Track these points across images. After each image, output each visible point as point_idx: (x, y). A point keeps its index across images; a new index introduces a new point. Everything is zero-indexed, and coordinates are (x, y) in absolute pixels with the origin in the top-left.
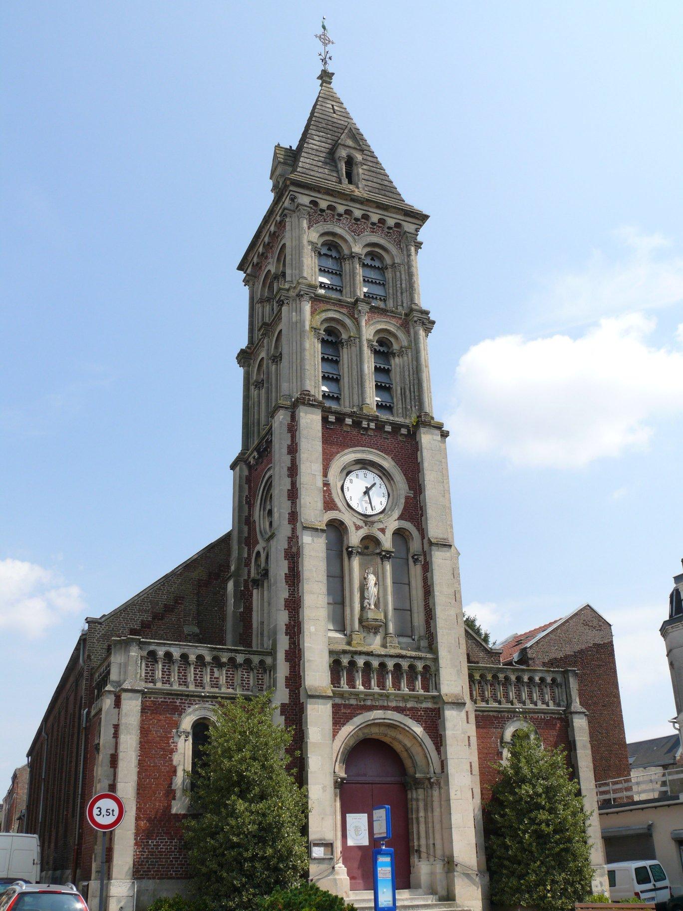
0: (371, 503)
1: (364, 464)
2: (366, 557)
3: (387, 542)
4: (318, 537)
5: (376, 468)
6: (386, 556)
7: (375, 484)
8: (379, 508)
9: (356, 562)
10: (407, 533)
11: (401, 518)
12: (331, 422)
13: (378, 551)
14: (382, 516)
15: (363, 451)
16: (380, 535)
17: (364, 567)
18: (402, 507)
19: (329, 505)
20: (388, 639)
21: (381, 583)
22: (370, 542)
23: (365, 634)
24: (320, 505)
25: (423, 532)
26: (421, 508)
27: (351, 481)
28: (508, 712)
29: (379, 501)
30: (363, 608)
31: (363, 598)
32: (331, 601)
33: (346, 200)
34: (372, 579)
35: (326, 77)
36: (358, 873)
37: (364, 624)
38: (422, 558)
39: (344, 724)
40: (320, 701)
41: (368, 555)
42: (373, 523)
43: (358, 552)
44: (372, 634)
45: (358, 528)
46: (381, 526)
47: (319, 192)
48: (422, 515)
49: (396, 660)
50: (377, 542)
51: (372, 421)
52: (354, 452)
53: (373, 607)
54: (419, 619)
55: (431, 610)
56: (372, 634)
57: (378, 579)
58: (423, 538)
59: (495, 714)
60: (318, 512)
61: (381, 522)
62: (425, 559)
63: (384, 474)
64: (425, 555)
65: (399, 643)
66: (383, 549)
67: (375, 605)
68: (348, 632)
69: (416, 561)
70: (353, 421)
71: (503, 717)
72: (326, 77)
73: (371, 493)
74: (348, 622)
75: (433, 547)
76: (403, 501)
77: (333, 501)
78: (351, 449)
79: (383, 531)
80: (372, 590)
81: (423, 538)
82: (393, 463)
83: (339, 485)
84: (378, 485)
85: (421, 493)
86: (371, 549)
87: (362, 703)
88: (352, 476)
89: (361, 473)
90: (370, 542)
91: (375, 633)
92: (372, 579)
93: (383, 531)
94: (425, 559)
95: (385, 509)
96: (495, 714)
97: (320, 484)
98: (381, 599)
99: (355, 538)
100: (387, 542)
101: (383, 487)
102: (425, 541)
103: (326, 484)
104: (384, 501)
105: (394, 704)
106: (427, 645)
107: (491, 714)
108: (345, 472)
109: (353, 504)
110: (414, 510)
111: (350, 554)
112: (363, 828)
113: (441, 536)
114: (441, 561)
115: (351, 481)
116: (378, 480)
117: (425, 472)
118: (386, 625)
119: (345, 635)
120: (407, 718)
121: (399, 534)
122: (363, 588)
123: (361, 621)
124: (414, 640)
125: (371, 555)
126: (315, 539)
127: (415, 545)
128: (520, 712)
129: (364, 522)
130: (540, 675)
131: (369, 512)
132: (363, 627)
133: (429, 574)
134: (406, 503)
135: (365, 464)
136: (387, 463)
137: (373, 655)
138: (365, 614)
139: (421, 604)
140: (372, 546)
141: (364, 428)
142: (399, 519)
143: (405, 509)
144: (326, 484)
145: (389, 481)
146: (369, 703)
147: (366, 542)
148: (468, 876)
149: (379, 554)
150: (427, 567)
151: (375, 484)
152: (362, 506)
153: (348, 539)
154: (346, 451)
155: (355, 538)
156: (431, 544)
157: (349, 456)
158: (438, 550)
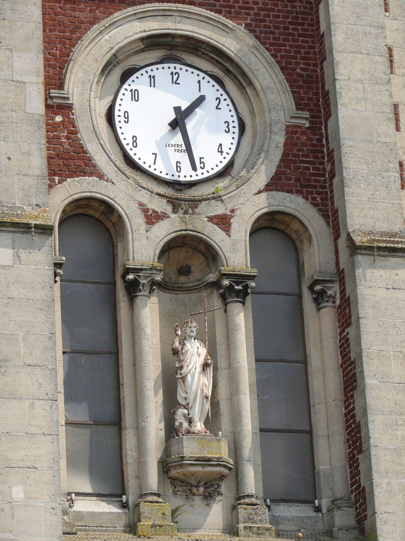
0: (189, 150)
1: (171, 48)
2: (183, 296)
3: (235, 252)
4: (31, 246)
5: (202, 55)
6: (235, 289)
7: (200, 100)
8: (214, 163)
9: (150, 312)
10: (295, 226)
11: (274, 185)
13: (212, 277)
14: (222, 184)
15: (165, 14)
16: (215, 236)
17: (172, 323)
18: (276, 156)
19: (67, 158)
20: (242, 512)
21: (222, 363)
22: (188, 255)
23: (177, 501)
24: (38, 162)
25: (332, 214)
26: (331, 154)
27: (135, 96)
29: (213, 141)
30: (171, 431)
31: (171, 403)
32: (83, 416)
34: (195, 353)
37: (173, 473)
38: (334, 290)
41: (188, 290)
42: (195, 203)
43: (153, 283)
44: (198, 501)
45: (152, 218)
46: (219, 209)
48: (333, 175)
50: (210, 254)
52: (141, 17)
53: (199, 426)
54: (329, 454)
55: (358, 425)
56: (198, 501)
57: (212, 352)
58: (337, 236)
60: (31, 181)
61: (218, 198)
62: (343, 292)
63: (228, 72)
64: (342, 281)
65: (274, 520)
66: (224, 269)
67: (207, 423)
68: (131, 497)
69: (319, 298)
73: (190, 124)
74: (130, 471)
75: (360, 259)
76: (280, 139)
77: (80, 151)
78: (130, 10)
79: (223, 222)
80: (197, 382)
81: (337, 236)
82: (250, 40)
83: (101, 108)
84: (210, 102)
85: (328, 115)
86: (196, 274)
88: (138, 82)
89: (162, 73)
90: (188, 255)
91: (208, 497)
92: (195, 353)
93: (223, 222)
94: (343, 292)
95: (230, 165)
97: (36, 104)
98: (224, 406)
99: (143, 246)
100: (235, 252)
101: (226, 107)
102: (342, 242)
103: (58, 107)
104: (229, 141)
106: (351, 521)
108: (117, 73)
109: (142, 156)
110: (310, 162)
111: (132, 288)
113: (384, 227)
114: (382, 293)
115: (135, 96)
116: (210, 89)
117: (338, 57)
118: (236, 472)
119: (124, 506)
121: (270, 226)
122: (172, 380)
123: (165, 466)
124: (318, 510)
125: (198, 288)
126: (23, 254)
127: (317, 257)
129: (171, 201)
131: (187, 174)
132: (174, 481)
133: (351, 330)
134: (289, 144)
135: (172, 47)
136: (234, 40)
138: (174, 448)
139: (337, 411)
140: (197, 264)
142: (269, 187)
143: (285, 160)
144: (58, 107)
145: (241, 88)
147: (180, 256)
149: (216, 285)
150: (346, 315)
151: (200, 100)
152: (167, 161)
153: (126, 249)
154: (117, 15)
155: (143, 246)
156: (354, 249)
157: (126, 29)
158: (373, 265)
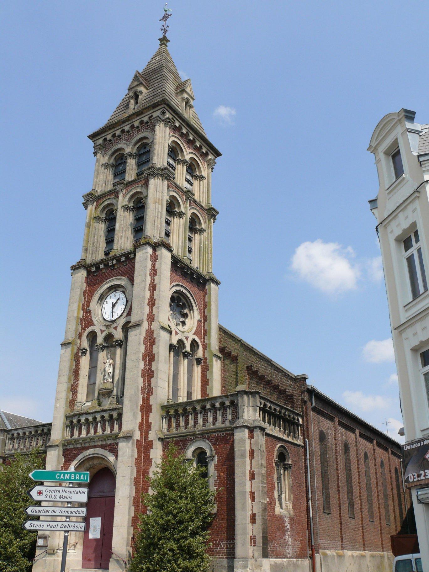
12: (94, 272)
28: (190, 435)
33: (121, 125)
35: (164, 40)
36: (92, 556)
39: (73, 461)
40: (53, 448)
45: (102, 331)
47: (106, 131)
49: (102, 414)
51: (113, 259)
59: (181, 438)
70: (104, 265)
71: (187, 440)
72: (164, 40)
87: (83, 445)
96: (181, 438)
105: (100, 443)
107: (179, 439)
112: (98, 527)
120: (107, 451)
128: (199, 434)
130: (220, 400)
135: (115, 288)
137: (89, 413)
141: (111, 266)
146: (87, 445)
148: (117, 561)
151: (119, 299)
